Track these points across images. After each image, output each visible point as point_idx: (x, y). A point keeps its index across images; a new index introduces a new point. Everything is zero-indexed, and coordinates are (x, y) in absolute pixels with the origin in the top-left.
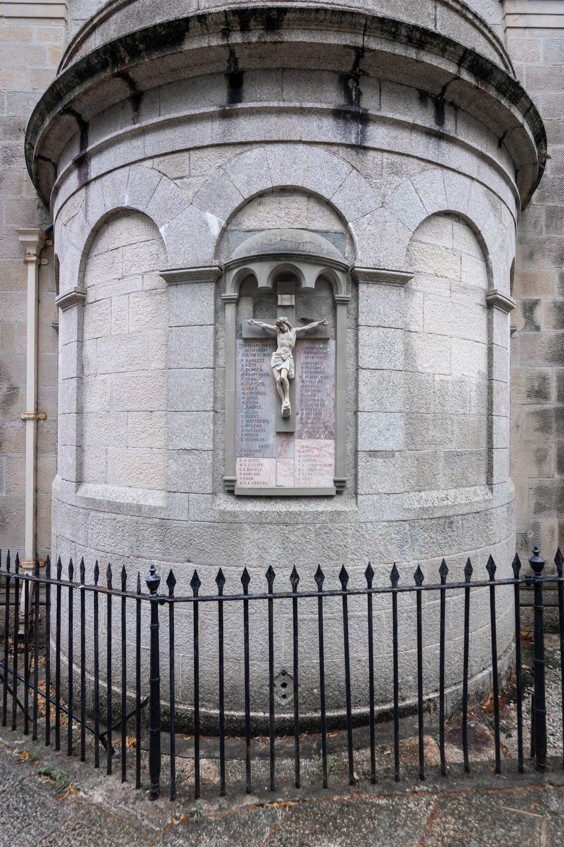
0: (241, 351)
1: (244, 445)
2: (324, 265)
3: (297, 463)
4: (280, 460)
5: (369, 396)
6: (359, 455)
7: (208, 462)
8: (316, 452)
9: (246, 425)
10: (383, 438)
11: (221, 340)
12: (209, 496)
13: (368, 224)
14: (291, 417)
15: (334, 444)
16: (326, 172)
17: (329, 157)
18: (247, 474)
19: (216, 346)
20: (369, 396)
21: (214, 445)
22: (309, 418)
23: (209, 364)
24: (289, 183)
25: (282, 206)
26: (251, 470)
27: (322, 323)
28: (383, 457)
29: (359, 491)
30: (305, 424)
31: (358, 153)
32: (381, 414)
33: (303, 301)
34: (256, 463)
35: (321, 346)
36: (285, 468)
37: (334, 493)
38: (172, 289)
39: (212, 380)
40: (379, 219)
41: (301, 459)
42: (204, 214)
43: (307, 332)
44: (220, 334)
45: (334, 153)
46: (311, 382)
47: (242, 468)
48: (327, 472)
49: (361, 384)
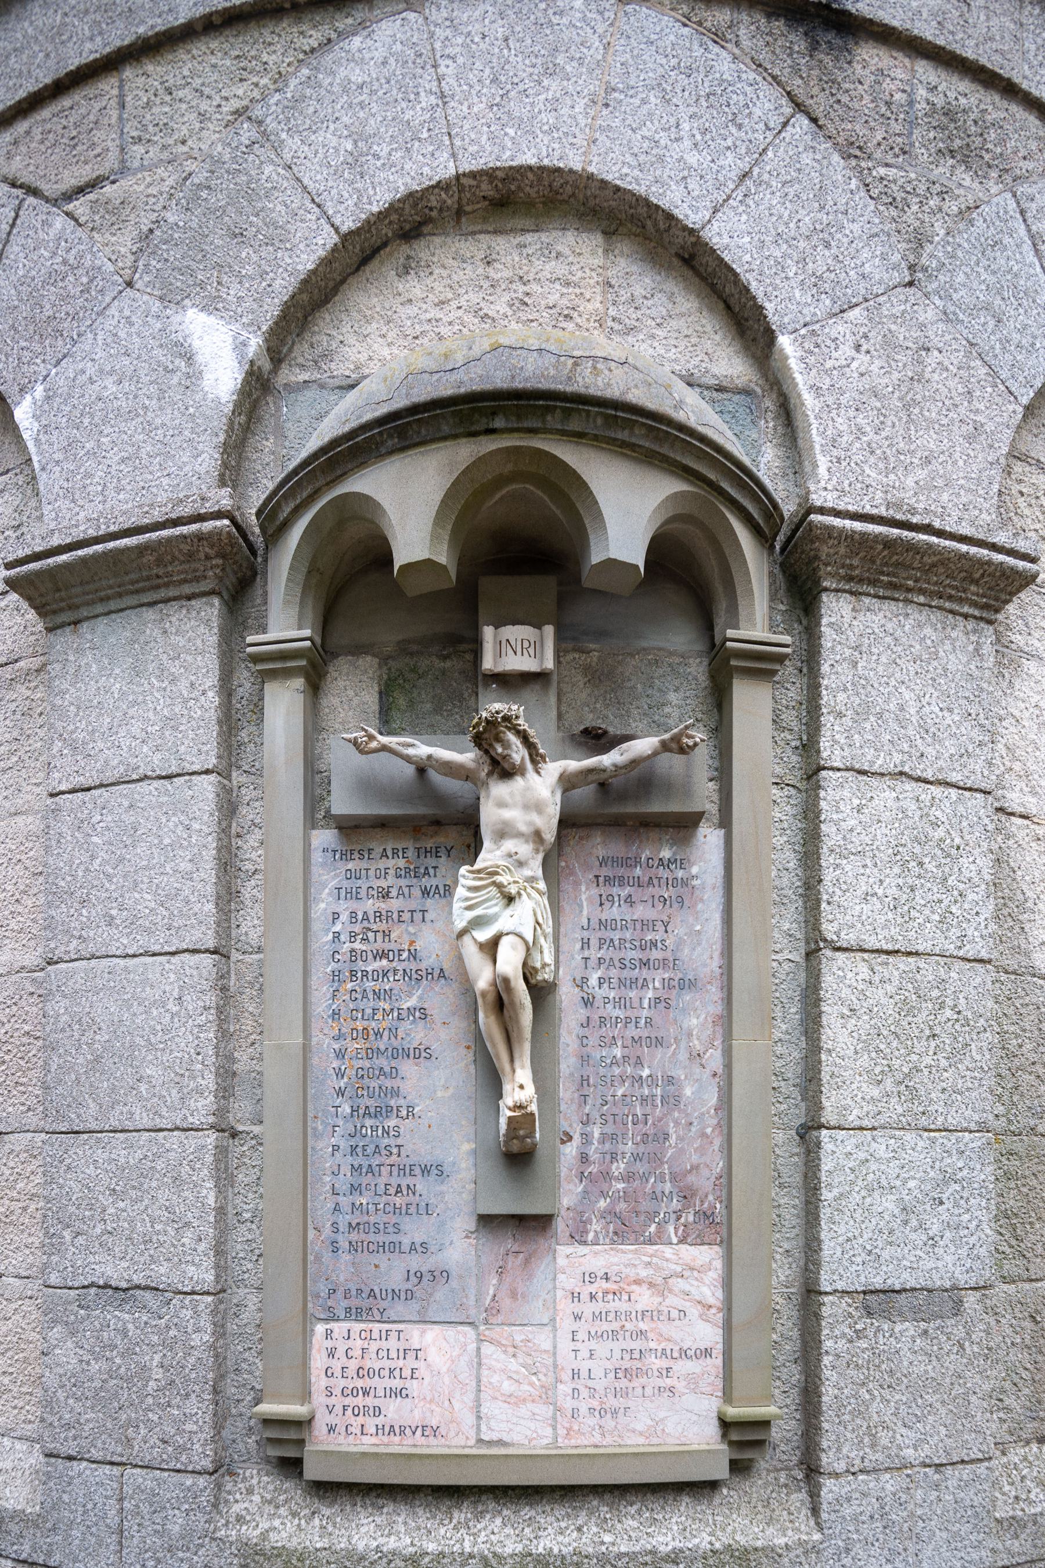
0: (328, 878)
1: (342, 1269)
2: (687, 473)
3: (565, 1345)
4: (495, 1333)
5: (864, 1061)
6: (825, 1311)
7: (196, 1340)
8: (645, 1299)
9: (354, 1188)
10: (919, 1238)
11: (253, 839)
12: (202, 1481)
13: (858, 347)
14: (542, 1153)
15: (718, 1264)
16: (684, 113)
17: (698, 52)
18: (354, 1392)
19: (228, 863)
20: (864, 1061)
21: (221, 1269)
22: (614, 1157)
23: (197, 934)
24: (529, 158)
25: (500, 272)
26: (370, 1373)
27: (676, 739)
28: (917, 1315)
29: (824, 1459)
30: (596, 1181)
31: (814, 47)
32: (909, 1137)
33: (587, 669)
34: (393, 1344)
35: (666, 853)
36: (513, 1365)
37: (720, 1471)
38: (64, 639)
39: (211, 999)
40: (901, 332)
41: (583, 1328)
42: (176, 319)
43: (604, 784)
44: (247, 814)
45: (718, 38)
46: (621, 1002)
47: (336, 1366)
48: (693, 1381)
49: (830, 1012)
